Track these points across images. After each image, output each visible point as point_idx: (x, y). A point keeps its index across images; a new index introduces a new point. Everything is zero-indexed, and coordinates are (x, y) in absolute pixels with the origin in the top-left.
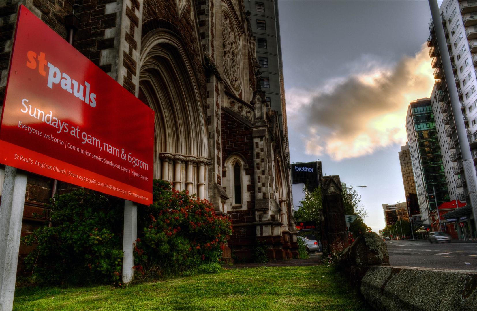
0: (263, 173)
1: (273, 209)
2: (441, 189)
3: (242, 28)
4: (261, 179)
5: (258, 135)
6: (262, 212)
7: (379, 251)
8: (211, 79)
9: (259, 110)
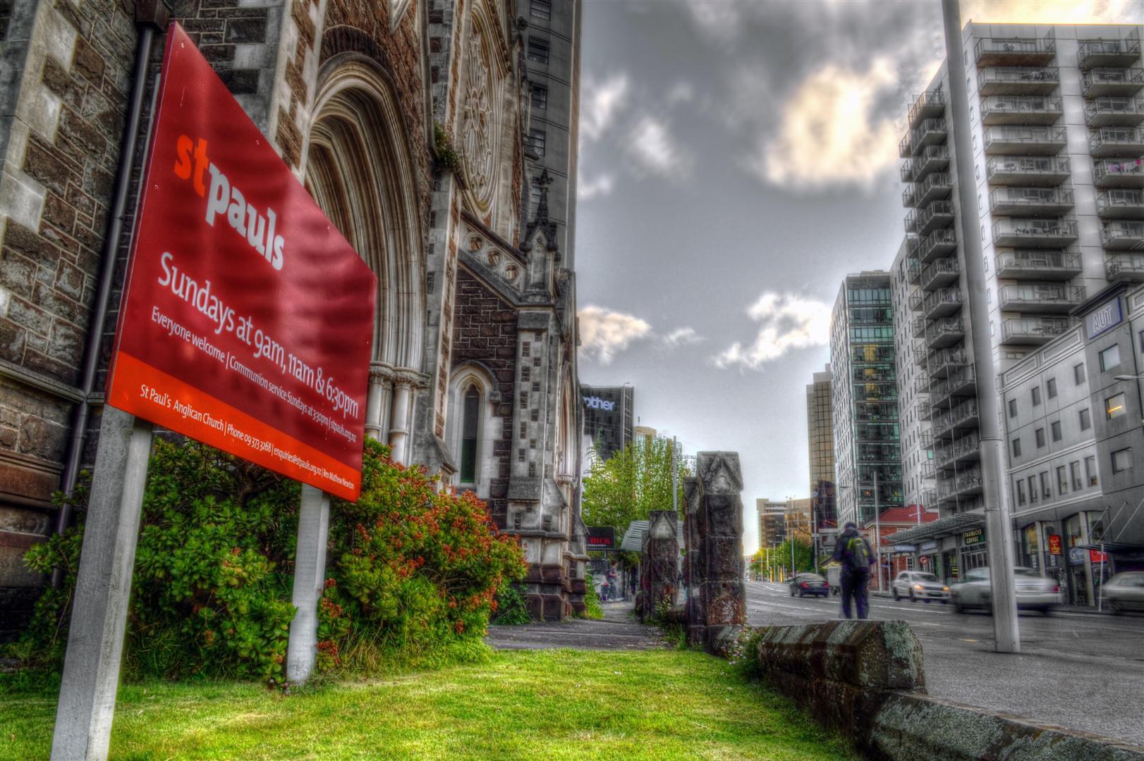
0: (535, 417)
1: (549, 502)
2: (889, 477)
3: (507, 60)
4: (528, 430)
5: (532, 326)
6: (523, 508)
7: (911, 659)
8: (443, 181)
9: (539, 267)
